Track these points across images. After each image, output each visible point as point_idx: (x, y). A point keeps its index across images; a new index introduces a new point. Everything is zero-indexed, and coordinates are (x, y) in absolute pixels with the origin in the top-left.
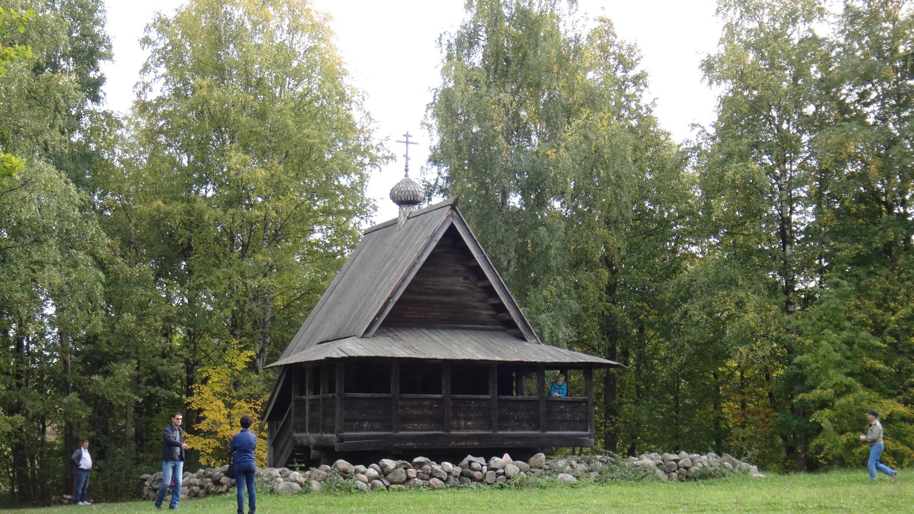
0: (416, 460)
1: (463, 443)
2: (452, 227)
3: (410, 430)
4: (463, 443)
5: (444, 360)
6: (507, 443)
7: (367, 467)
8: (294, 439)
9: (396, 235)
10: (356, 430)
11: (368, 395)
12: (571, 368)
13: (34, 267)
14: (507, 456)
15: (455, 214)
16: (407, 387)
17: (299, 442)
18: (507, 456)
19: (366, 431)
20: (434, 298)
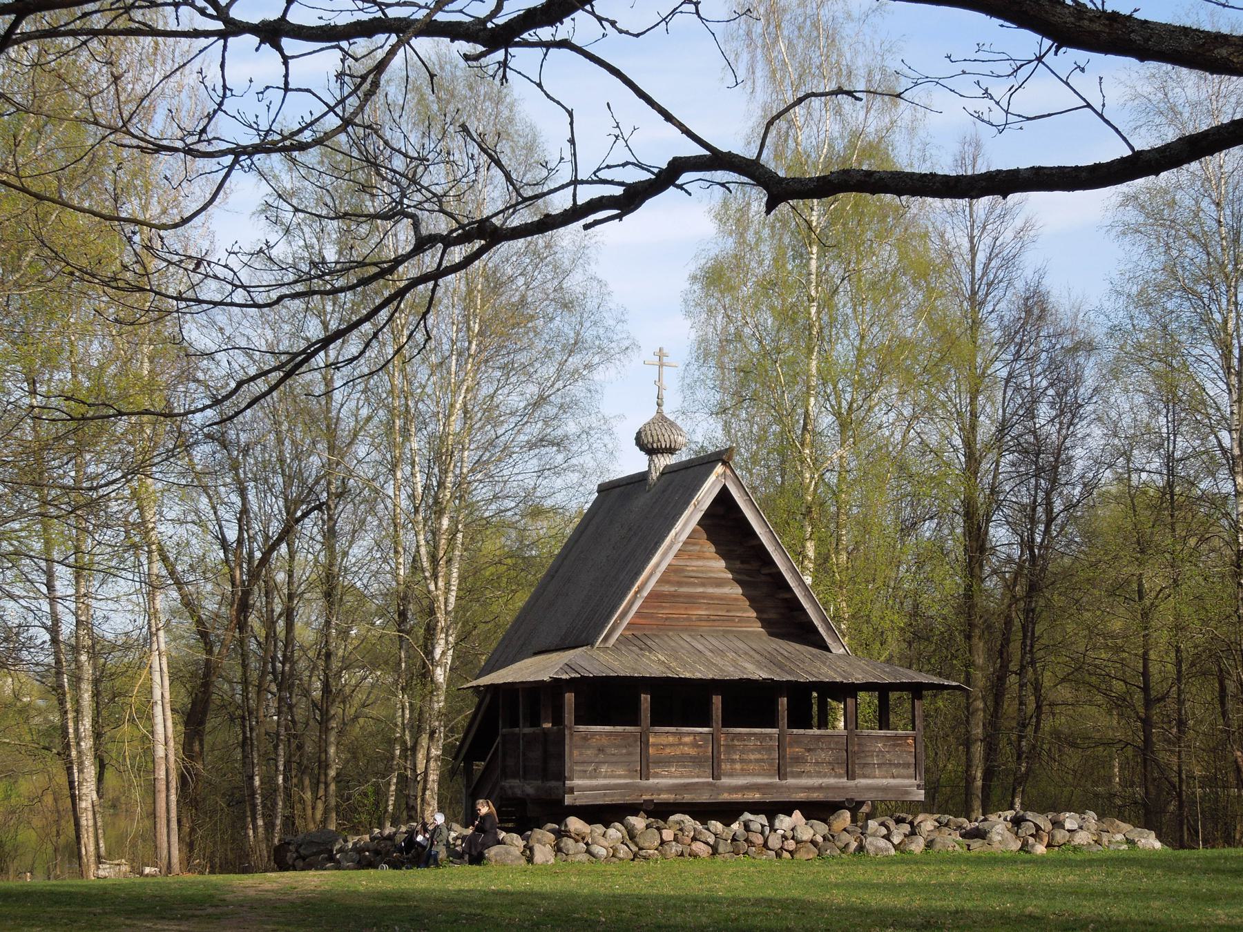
0: (672, 818)
1: (815, 795)
2: (724, 490)
3: (665, 777)
4: (815, 795)
5: (713, 680)
6: (801, 796)
7: (607, 826)
8: (502, 788)
9: (641, 501)
10: (591, 778)
11: (608, 728)
12: (928, 689)
13: (998, 212)
14: (797, 814)
15: (728, 472)
16: (662, 717)
17: (510, 792)
18: (797, 814)
19: (605, 777)
20: (700, 590)
